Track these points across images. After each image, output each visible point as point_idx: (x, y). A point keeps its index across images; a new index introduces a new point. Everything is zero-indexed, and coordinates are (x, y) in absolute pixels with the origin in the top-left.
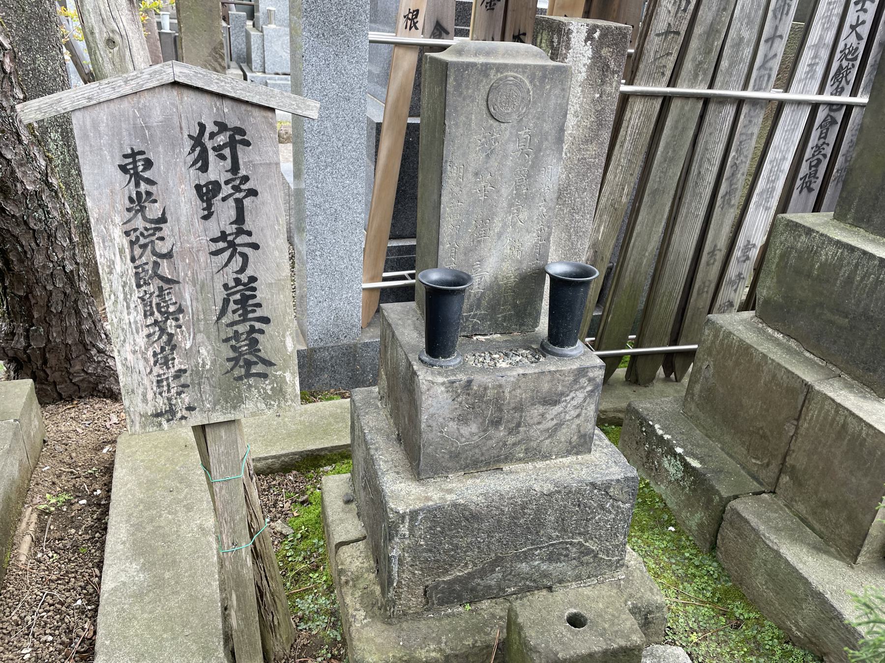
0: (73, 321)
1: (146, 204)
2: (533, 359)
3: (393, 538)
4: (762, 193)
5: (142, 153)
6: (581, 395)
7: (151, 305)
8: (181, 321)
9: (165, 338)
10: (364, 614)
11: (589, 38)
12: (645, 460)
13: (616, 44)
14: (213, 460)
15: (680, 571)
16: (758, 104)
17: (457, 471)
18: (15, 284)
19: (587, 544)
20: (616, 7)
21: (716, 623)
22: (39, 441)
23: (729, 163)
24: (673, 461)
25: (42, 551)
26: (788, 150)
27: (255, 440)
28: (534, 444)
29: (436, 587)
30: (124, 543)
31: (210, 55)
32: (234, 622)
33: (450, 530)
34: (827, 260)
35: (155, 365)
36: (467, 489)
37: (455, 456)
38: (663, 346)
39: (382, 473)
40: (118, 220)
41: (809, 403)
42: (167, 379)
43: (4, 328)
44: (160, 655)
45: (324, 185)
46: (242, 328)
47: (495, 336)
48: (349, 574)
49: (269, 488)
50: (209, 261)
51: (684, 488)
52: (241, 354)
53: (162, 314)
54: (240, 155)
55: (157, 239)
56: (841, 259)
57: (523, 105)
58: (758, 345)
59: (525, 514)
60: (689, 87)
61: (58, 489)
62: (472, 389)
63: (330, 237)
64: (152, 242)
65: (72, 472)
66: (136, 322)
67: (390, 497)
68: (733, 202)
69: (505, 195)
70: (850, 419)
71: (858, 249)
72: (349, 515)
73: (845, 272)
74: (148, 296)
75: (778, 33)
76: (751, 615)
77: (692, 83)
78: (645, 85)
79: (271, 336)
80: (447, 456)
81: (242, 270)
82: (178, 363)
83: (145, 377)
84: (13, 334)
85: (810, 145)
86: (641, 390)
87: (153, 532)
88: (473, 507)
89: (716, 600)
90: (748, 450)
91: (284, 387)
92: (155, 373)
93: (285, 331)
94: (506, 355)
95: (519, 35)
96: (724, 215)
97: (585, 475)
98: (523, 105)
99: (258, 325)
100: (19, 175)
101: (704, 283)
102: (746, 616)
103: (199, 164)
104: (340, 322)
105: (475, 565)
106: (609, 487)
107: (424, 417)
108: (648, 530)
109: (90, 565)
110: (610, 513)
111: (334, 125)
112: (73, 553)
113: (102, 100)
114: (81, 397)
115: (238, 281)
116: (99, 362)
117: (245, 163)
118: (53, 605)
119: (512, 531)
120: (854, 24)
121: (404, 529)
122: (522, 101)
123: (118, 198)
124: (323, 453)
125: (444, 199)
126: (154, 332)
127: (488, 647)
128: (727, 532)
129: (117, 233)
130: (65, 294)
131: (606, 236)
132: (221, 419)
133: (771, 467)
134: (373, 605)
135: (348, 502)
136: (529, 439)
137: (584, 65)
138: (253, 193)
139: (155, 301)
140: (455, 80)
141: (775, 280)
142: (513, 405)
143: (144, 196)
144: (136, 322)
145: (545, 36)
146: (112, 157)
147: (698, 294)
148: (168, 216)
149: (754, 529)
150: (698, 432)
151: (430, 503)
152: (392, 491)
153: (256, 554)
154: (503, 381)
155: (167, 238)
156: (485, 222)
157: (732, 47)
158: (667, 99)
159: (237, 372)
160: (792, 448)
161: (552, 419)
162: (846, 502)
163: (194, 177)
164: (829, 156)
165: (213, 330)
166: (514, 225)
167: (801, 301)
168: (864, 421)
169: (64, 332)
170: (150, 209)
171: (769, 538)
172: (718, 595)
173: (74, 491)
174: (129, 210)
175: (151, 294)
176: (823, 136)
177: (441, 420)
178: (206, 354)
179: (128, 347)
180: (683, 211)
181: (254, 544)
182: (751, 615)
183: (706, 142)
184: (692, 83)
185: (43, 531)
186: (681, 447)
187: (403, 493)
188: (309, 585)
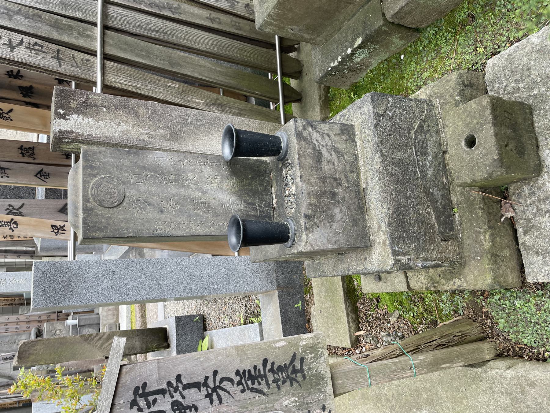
2: (290, 167)
3: (410, 266)
6: (315, 135)
11: (64, 117)
12: (354, 73)
13: (68, 97)
17: (365, 221)
19: (416, 127)
21: (471, 33)
23: (149, 10)
24: (356, 55)
27: (337, 328)
28: (348, 167)
29: (442, 233)
36: (378, 214)
38: (276, 54)
39: (366, 270)
44: (478, 408)
45: (171, 285)
46: (271, 378)
47: (273, 191)
48: (429, 285)
49: (368, 321)
50: (226, 404)
51: (375, 49)
52: (288, 377)
57: (112, 182)
59: (395, 174)
60: (97, 41)
62: (311, 214)
68: (177, 6)
69: (176, 190)
72: (389, 279)
76: (466, 7)
77: (93, 38)
79: (276, 357)
80: (356, 228)
81: (231, 381)
86: (305, 69)
87: (396, 400)
88: (391, 212)
89: (454, 31)
90: (350, 3)
93: (272, 348)
94: (286, 185)
95: (65, 155)
96: (186, 12)
97: (369, 131)
98: (112, 182)
99: (269, 367)
101: (233, 26)
102: (466, 10)
104: (260, 270)
105: (428, 207)
106: (378, 114)
107: (330, 247)
108: (403, 74)
110: (395, 112)
111: (131, 280)
115: (239, 383)
117: (158, 385)
119: (407, 182)
121: (404, 259)
122: (109, 182)
124: (346, 286)
127: (483, 199)
128: (408, 21)
132: (331, 387)
134: (451, 272)
135: (380, 279)
136: (345, 171)
137: (83, 120)
138: (179, 378)
140: (95, 232)
142: (322, 184)
145: (65, 146)
147: (240, 30)
149: (407, 4)
150: (336, 36)
151: (388, 241)
152: (379, 265)
153: (417, 350)
154: (305, 192)
157: (67, 9)
158: (106, 57)
159: (300, 379)
161: (331, 155)
165: (271, 397)
166: (197, 182)
172: (450, 29)
177: (331, 234)
178: (288, 401)
180: (183, 42)
181: (407, 353)
182: (466, 7)
183: (135, 27)
186: (347, 49)
187: (380, 258)
188: (433, 305)
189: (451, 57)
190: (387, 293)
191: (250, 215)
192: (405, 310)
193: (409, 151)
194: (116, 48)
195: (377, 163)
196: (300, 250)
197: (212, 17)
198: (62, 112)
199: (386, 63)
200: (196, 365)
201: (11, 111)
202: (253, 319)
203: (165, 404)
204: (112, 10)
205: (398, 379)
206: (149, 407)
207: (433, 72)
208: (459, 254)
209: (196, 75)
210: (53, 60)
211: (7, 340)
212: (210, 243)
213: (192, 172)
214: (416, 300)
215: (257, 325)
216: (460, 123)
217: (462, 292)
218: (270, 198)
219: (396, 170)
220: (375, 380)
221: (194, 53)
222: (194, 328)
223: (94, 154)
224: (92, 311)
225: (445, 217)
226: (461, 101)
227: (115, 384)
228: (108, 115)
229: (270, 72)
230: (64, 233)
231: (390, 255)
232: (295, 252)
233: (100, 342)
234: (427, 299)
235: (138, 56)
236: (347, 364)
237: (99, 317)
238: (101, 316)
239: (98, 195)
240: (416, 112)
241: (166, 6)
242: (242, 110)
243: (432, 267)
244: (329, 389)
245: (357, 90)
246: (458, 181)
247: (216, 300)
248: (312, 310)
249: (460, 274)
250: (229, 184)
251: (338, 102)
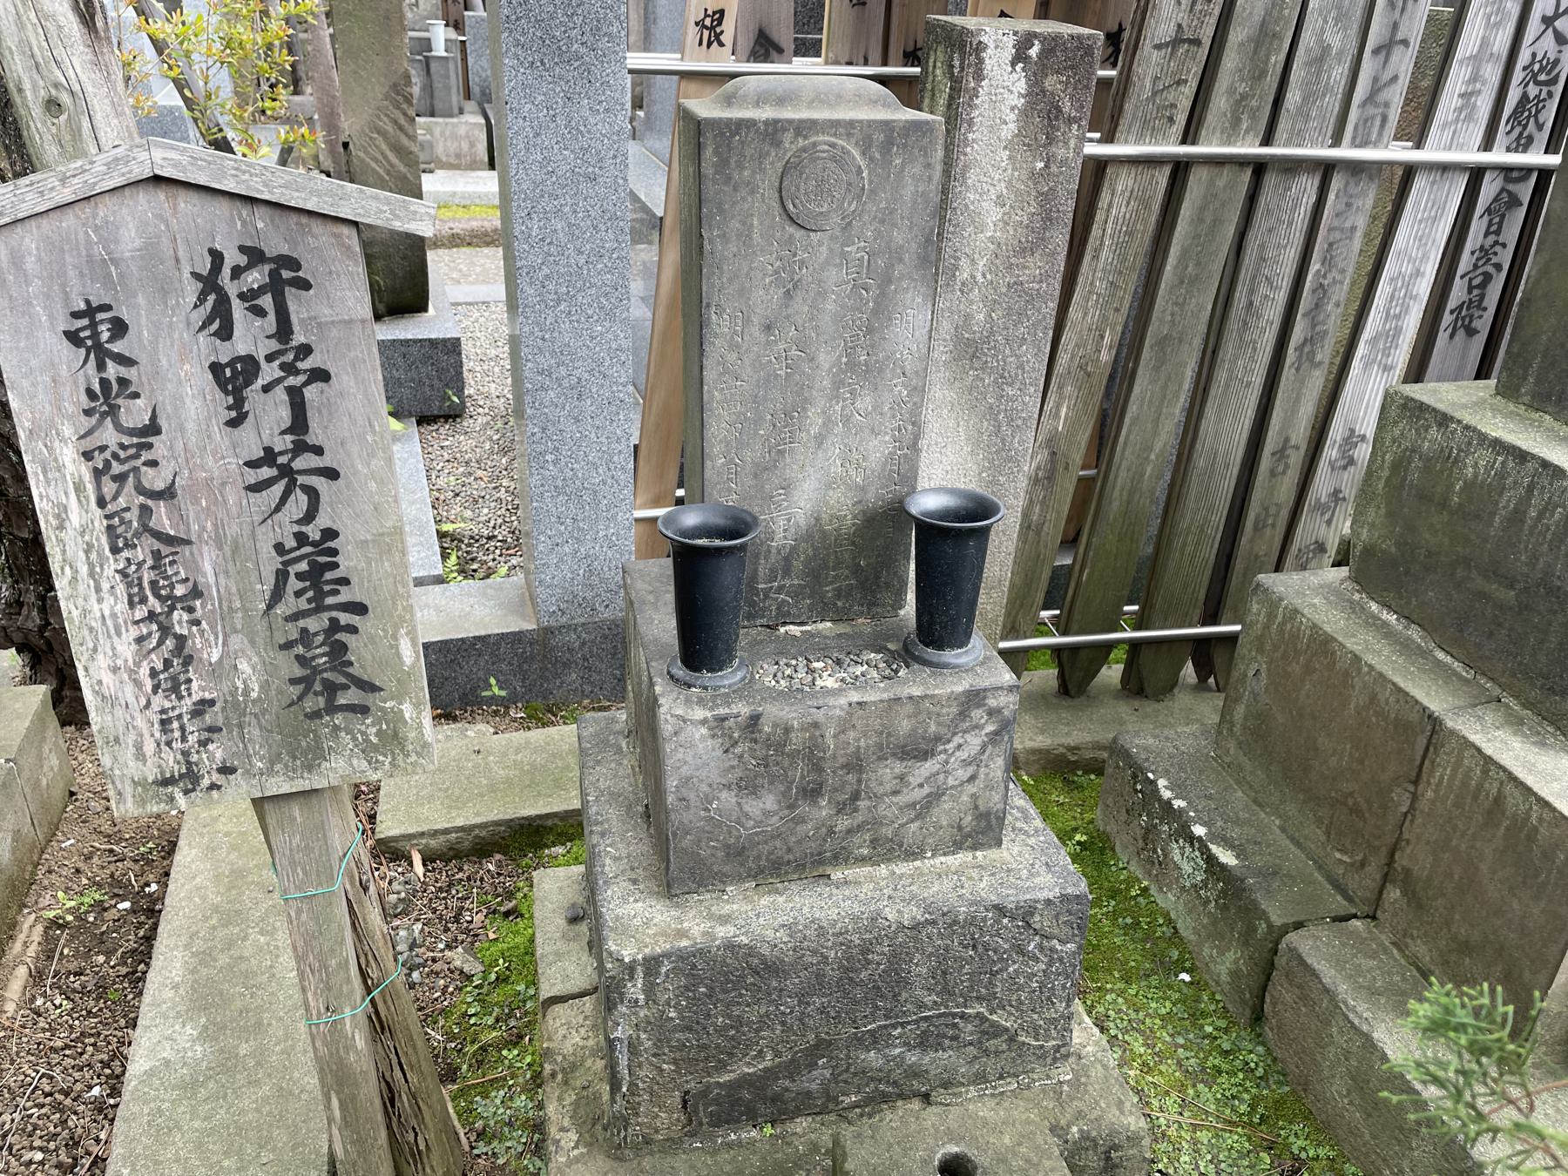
1: (120, 401)
2: (888, 671)
3: (615, 1005)
4: (1374, 340)
5: (106, 308)
6: (974, 741)
7: (140, 585)
8: (199, 613)
9: (170, 643)
10: (575, 1138)
11: (1020, 56)
12: (1141, 844)
13: (1072, 67)
15: (1192, 1061)
16: (1362, 171)
17: (739, 879)
18: (14, 518)
19: (994, 1017)
22: (58, 793)
23: (1308, 284)
24: (1188, 850)
25: (44, 995)
26: (1425, 257)
28: (888, 832)
29: (704, 1094)
30: (176, 987)
31: (386, 97)
33: (726, 991)
34: (1476, 475)
35: (155, 692)
36: (758, 916)
37: (737, 853)
38: (1190, 626)
40: (67, 430)
41: (1436, 752)
42: (180, 717)
43: (5, 593)
46: (314, 624)
47: (820, 626)
48: (559, 1059)
49: (451, 885)
50: (244, 502)
51: (1207, 902)
52: (316, 671)
53: (164, 602)
54: (292, 306)
55: (144, 464)
56: (1502, 475)
57: (849, 197)
58: (1345, 635)
59: (869, 962)
60: (1223, 144)
61: (85, 881)
62: (760, 731)
63: (570, 428)
64: (136, 470)
65: (111, 851)
66: (114, 616)
67: (612, 929)
68: (1319, 357)
70: (1509, 788)
71: (1533, 456)
73: (1509, 500)
74: (133, 568)
75: (1399, 36)
76: (1322, 1152)
77: (1230, 136)
78: (1137, 142)
79: (372, 638)
80: (720, 854)
81: (309, 517)
82: (198, 689)
83: (137, 714)
84: (20, 604)
85: (1469, 245)
86: (1149, 707)
87: (230, 967)
88: (765, 950)
90: (1328, 834)
91: (402, 731)
92: (156, 707)
93: (396, 628)
94: (839, 662)
95: (916, 49)
96: (1303, 383)
97: (985, 889)
98: (849, 197)
99: (344, 618)
101: (1266, 509)
102: (1311, 1153)
103: (215, 326)
105: (777, 1054)
106: (1032, 914)
107: (671, 783)
108: (1139, 979)
109: (122, 1022)
110: (1037, 960)
111: (570, 225)
112: (97, 1000)
113: (20, 216)
115: (301, 539)
117: (302, 321)
118: (51, 1094)
119: (846, 994)
120: (1550, 13)
121: (636, 990)
123: (66, 391)
124: (549, 823)
125: (710, 375)
126: (150, 634)
128: (1281, 993)
131: (1072, 423)
132: (286, 788)
133: (1368, 869)
134: (595, 1121)
135: (574, 920)
136: (877, 823)
137: (1012, 109)
138: (321, 375)
139: (147, 576)
140: (716, 152)
141: (1383, 511)
142: (842, 760)
143: (115, 386)
144: (114, 616)
146: (51, 317)
147: (1256, 529)
148: (163, 422)
149: (1327, 991)
150: (1240, 794)
151: (684, 943)
152: (617, 918)
153: (378, 1025)
154: (819, 716)
155: (163, 463)
156: (792, 415)
157: (1308, 64)
158: (1180, 169)
159: (309, 704)
160: (1406, 836)
161: (921, 786)
162: (1502, 947)
163: (207, 348)
164: (1506, 267)
165: (261, 626)
166: (847, 420)
167: (1430, 554)
168: (1535, 794)
170: (128, 409)
171: (1353, 1010)
173: (110, 885)
175: (140, 565)
176: (1494, 230)
177: (704, 788)
178: (249, 671)
179: (102, 661)
180: (1221, 375)
181: (372, 1001)
182: (1322, 1152)
184: (1230, 136)
185: (50, 958)
186: (1204, 824)
187: (637, 922)
188: (500, 1071)
189: (1186, 1114)
190: (532, 940)
191: (756, 563)
192: (484, 991)
193: (930, 999)
194: (1205, 197)
195: (899, 911)
196: (662, 701)
197: (1289, 451)
198: (1034, 52)
199: (1169, 931)
200: (353, 421)
202: (453, 559)
203: (250, 339)
205: (301, 974)
207: (1144, 1064)
208: (648, 1141)
209: (1133, 409)
212: (677, 453)
213: (874, 408)
214: (512, 1023)
215: (439, 570)
216: (1007, 1140)
217: (539, 1150)
218: (804, 618)
219: (879, 964)
220: (299, 911)
221: (1192, 404)
222: (429, 391)
223: (924, 151)
224: (468, 96)
225: (750, 1101)
226: (1066, 1142)
227: (309, 207)
228: (1024, 175)
229: (1142, 609)
230: (700, 44)
231: (647, 951)
232: (658, 689)
233: (389, 128)
234: (516, 1052)
235: (1185, 252)
236: (344, 836)
237: (451, 116)
238: (455, 120)
239: (814, 160)
240: (1036, 1016)
241: (1318, 329)
242: (1038, 532)
243: (612, 1067)
244: (279, 785)
245: (1093, 853)
246: (849, 1135)
247: (504, 451)
248: (481, 727)
249: (591, 1145)
251: (1061, 799)
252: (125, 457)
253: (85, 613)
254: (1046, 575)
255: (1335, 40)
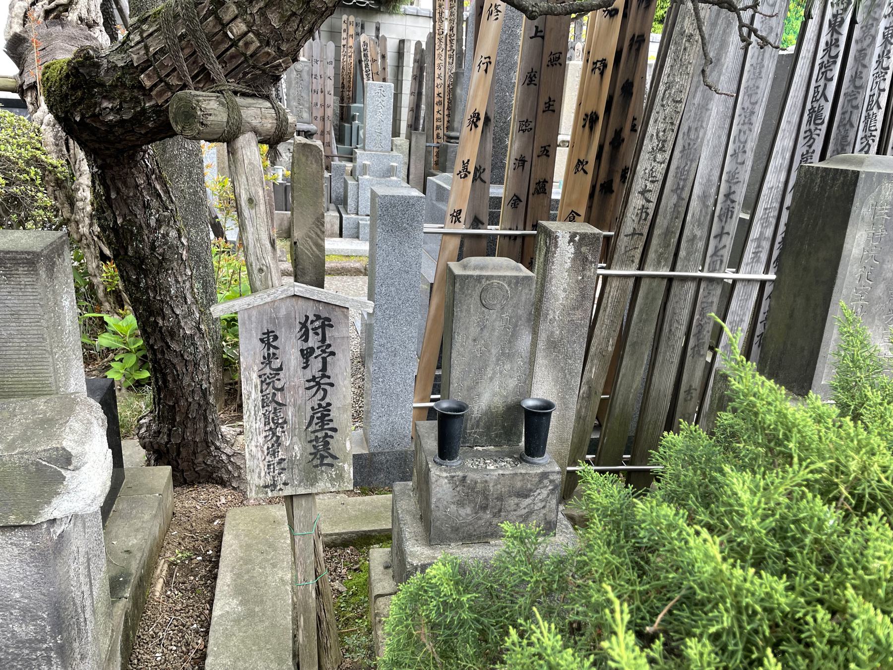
0: (202, 425)
6: (545, 492)
9: (274, 438)
11: (572, 240)
14: (296, 521)
17: (456, 541)
20: (612, 203)
22: (171, 513)
26: (744, 314)
30: (228, 586)
32: (300, 638)
37: (456, 530)
40: (256, 369)
46: (320, 435)
49: (332, 557)
52: (318, 451)
63: (390, 368)
72: (387, 577)
75: (725, 231)
82: (281, 455)
94: (496, 461)
96: (695, 362)
99: (330, 433)
100: (182, 324)
104: (395, 433)
107: (434, 500)
114: (199, 483)
115: (320, 406)
116: (215, 456)
129: (254, 376)
130: (199, 404)
132: (303, 492)
135: (387, 567)
138: (333, 354)
139: (271, 416)
142: (495, 496)
148: (284, 367)
153: (318, 592)
154: (487, 478)
156: (482, 370)
157: (688, 241)
158: (638, 279)
163: (300, 344)
165: (303, 434)
166: (501, 373)
169: (195, 432)
174: (262, 363)
179: (253, 443)
180: (660, 358)
181: (317, 582)
183: (674, 308)
185: (171, 576)
198: (577, 239)
201: (586, 172)
204: (691, 287)
206: (313, 329)
210: (632, 229)
211: (303, 94)
223: (529, 285)
235: (641, 311)
242: (584, 420)
250: (499, 403)
252: (271, 378)
253: (251, 427)
254: (587, 442)
255: (698, 233)
